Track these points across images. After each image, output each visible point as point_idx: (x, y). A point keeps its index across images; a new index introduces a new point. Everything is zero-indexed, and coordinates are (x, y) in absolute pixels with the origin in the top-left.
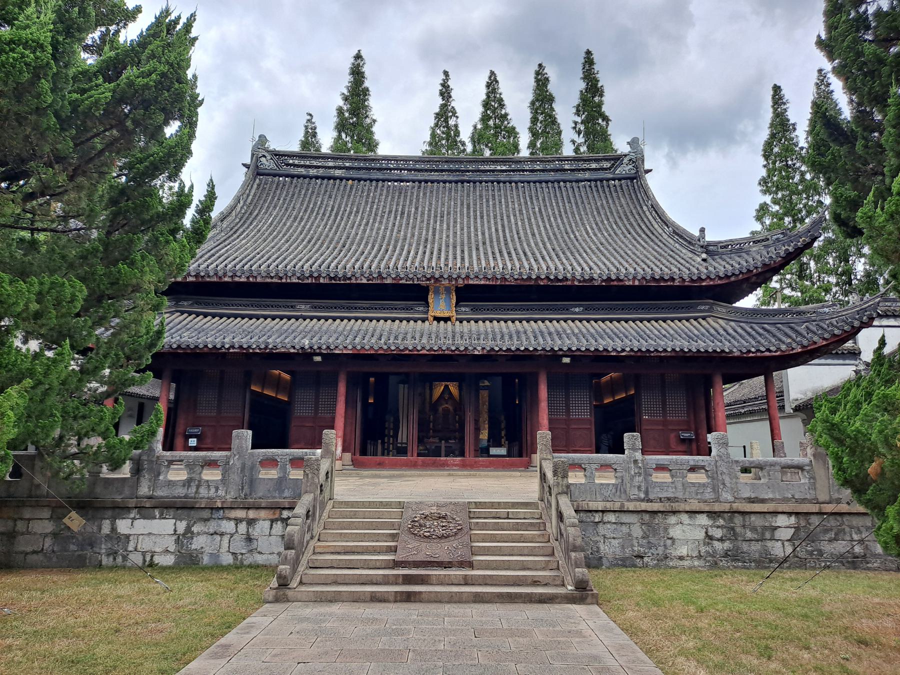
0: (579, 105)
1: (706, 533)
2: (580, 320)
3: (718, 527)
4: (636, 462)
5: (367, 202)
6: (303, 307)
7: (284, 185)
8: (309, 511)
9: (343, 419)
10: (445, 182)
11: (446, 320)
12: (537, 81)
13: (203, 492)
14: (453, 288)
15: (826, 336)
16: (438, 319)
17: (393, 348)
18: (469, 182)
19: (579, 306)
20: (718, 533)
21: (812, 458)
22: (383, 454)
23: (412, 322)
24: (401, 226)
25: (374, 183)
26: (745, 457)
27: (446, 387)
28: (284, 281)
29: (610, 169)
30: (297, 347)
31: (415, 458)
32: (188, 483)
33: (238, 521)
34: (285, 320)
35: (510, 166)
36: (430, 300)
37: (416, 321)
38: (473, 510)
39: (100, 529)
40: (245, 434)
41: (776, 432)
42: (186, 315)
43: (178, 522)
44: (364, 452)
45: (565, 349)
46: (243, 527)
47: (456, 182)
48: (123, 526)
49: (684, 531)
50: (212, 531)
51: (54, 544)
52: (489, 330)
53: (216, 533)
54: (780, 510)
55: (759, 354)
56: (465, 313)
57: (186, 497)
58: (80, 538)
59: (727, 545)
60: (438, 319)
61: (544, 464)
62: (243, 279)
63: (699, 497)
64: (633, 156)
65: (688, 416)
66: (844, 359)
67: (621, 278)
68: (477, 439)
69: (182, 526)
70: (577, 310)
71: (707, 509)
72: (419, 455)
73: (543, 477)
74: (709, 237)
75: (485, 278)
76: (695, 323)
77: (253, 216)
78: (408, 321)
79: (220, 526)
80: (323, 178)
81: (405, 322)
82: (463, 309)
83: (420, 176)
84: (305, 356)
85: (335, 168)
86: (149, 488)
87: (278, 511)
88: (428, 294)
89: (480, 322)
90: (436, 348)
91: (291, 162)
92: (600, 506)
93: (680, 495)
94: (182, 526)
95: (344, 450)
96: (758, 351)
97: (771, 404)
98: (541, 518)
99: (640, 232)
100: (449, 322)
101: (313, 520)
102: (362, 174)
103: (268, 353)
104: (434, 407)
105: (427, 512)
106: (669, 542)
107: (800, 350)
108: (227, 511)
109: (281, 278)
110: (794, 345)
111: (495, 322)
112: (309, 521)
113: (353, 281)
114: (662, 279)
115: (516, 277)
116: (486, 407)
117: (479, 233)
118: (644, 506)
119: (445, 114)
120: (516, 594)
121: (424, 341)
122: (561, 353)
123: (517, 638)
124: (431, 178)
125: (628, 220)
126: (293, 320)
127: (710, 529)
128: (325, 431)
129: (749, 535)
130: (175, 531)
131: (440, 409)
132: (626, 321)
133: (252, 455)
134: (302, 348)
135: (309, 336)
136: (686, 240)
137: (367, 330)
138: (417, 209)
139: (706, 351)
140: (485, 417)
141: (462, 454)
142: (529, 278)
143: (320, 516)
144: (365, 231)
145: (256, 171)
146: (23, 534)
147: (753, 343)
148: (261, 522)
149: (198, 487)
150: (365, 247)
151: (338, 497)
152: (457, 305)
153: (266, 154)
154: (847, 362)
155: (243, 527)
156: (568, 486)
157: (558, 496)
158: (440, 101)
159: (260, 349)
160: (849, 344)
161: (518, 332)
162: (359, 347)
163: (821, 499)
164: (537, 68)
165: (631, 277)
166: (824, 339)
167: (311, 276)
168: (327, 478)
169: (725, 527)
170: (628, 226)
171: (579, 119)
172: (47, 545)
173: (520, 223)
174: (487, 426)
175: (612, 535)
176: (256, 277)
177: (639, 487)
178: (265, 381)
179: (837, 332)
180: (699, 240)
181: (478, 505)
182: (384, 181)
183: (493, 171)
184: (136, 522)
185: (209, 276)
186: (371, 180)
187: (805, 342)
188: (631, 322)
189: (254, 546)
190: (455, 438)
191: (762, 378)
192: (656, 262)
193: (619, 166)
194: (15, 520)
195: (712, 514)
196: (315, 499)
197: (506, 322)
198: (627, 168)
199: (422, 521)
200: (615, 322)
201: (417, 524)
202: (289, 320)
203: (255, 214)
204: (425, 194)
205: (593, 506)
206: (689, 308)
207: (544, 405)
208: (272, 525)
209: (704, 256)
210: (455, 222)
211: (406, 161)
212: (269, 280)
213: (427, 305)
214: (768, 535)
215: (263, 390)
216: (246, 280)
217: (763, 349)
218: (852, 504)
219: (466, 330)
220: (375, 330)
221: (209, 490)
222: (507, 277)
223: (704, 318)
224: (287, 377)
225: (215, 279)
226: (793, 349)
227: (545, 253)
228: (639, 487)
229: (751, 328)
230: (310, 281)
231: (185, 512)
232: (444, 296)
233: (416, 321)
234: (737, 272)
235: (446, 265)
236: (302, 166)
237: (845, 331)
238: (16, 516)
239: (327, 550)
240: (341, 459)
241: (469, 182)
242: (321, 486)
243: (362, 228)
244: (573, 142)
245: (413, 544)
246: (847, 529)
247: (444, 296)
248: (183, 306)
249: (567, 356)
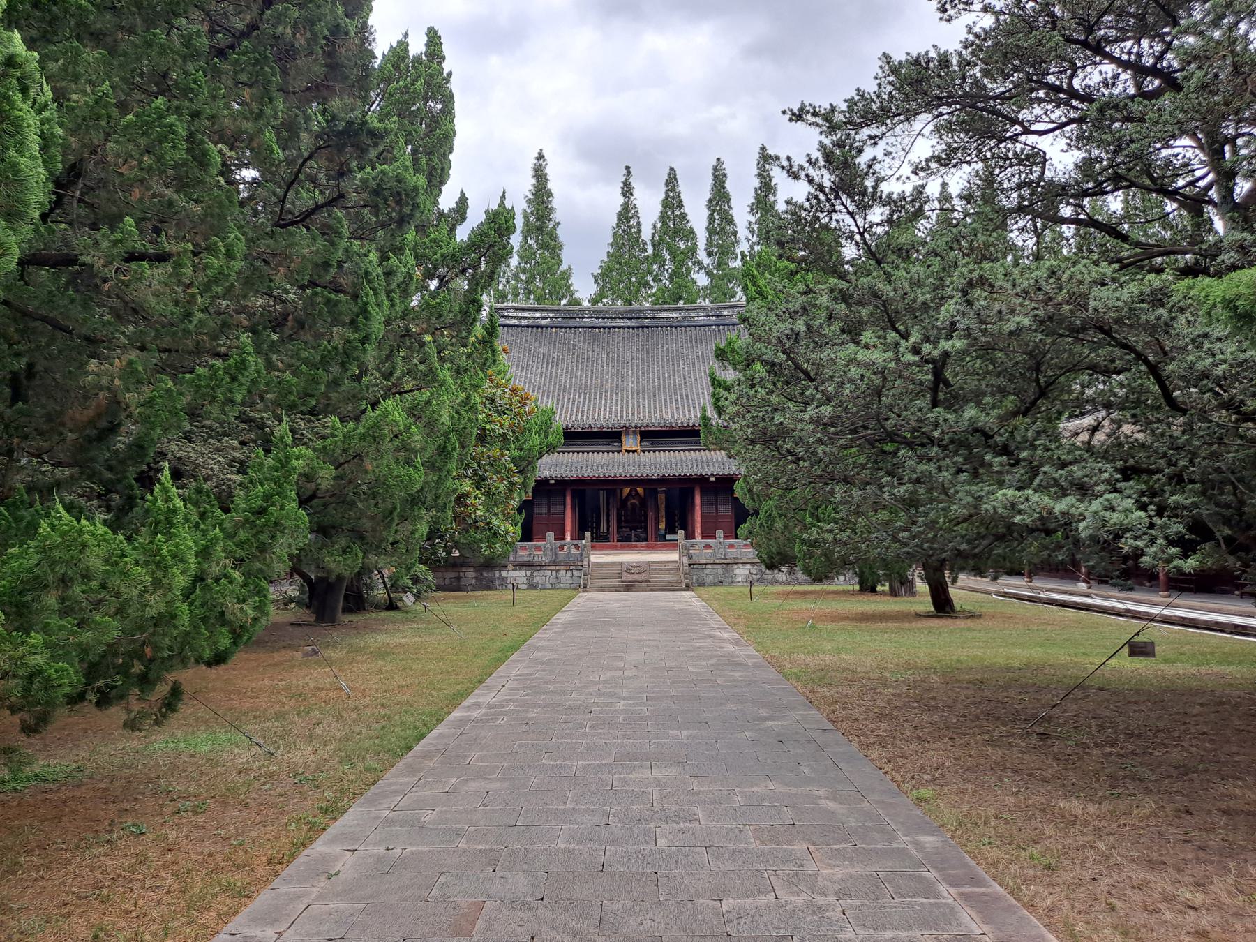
0: (753, 204)
11: (634, 452)
12: (715, 177)
16: (628, 451)
20: (755, 572)
31: (615, 543)
33: (552, 571)
38: (651, 565)
46: (554, 573)
48: (504, 574)
56: (646, 446)
59: (758, 576)
60: (628, 451)
68: (657, 529)
69: (529, 573)
80: (532, 327)
92: (705, 562)
94: (529, 573)
116: (663, 506)
118: (723, 561)
140: (663, 512)
142: (688, 426)
155: (554, 573)
158: (621, 200)
164: (715, 163)
171: (753, 219)
190: (641, 528)
205: (702, 561)
207: (698, 508)
244: (748, 240)
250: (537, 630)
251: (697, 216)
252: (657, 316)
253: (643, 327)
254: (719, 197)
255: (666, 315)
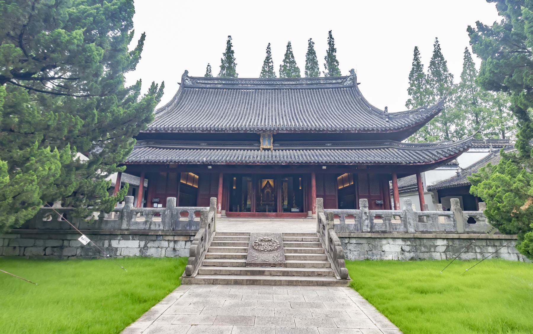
1: (402, 248)
2: (330, 150)
3: (407, 245)
4: (365, 213)
5: (232, 98)
6: (203, 144)
7: (196, 92)
8: (202, 237)
9: (221, 195)
10: (267, 89)
11: (268, 149)
13: (153, 227)
14: (272, 135)
15: (447, 155)
16: (264, 149)
17: (244, 162)
18: (278, 89)
19: (330, 143)
21: (454, 211)
22: (240, 211)
23: (253, 151)
24: (247, 109)
25: (235, 90)
26: (422, 210)
27: (268, 182)
28: (195, 132)
29: (341, 83)
30: (201, 162)
31: (254, 213)
32: (146, 222)
34: (195, 150)
35: (296, 82)
36: (261, 141)
37: (254, 150)
38: (284, 237)
39: (103, 245)
40: (173, 199)
41: (422, 200)
42: (151, 148)
43: (141, 242)
44: (231, 210)
45: (324, 162)
47: (272, 89)
48: (114, 243)
49: (390, 247)
50: (157, 246)
51: (81, 252)
52: (288, 154)
53: (159, 247)
54: (438, 237)
55: (415, 164)
57: (145, 229)
58: (94, 249)
60: (264, 149)
61: (320, 214)
62: (176, 132)
63: (397, 230)
64: (352, 77)
65: (380, 193)
66: (451, 167)
67: (350, 129)
69: (142, 244)
70: (329, 145)
71: (401, 237)
72: (256, 211)
73: (320, 221)
74: (390, 111)
75: (287, 130)
76: (383, 150)
77: (182, 105)
78: (251, 151)
79: (160, 244)
80: (213, 88)
81: (249, 151)
82: (276, 145)
83: (256, 87)
84: (204, 165)
85: (218, 84)
86: (127, 225)
87: (188, 237)
88: (260, 138)
89: (284, 151)
90: (264, 162)
91: (199, 82)
93: (388, 230)
94: (142, 244)
95: (222, 209)
96: (415, 162)
97: (420, 187)
98: (319, 241)
99: (356, 110)
100: (270, 151)
101: (205, 241)
102: (230, 87)
103: (187, 165)
104: (263, 190)
105: (262, 238)
106: (383, 253)
107: (434, 162)
108: (164, 236)
109: (193, 131)
110: (431, 160)
111: (291, 151)
112: (203, 242)
113: (226, 132)
114: (368, 130)
115: (301, 129)
116: (286, 190)
117: (283, 111)
119: (268, 60)
120: (309, 281)
121: (259, 158)
122: (322, 164)
123: (315, 309)
124: (261, 88)
125: (350, 105)
126: (199, 150)
127: (403, 247)
128: (211, 198)
129: (423, 249)
130: (139, 246)
131: (265, 191)
132: (352, 150)
133: (177, 209)
134: (203, 162)
135: (206, 157)
136: (378, 113)
137: (232, 154)
138: (254, 101)
139: (390, 163)
140: (286, 194)
141: (275, 211)
143: (209, 240)
144: (231, 111)
145: (183, 85)
146: (67, 247)
147: (412, 159)
148: (181, 242)
149: (150, 225)
150: (232, 117)
151: (218, 230)
152: (273, 143)
153: (188, 78)
154: (453, 168)
156: (334, 225)
157: (329, 230)
159: (184, 163)
160: (454, 161)
161: (302, 155)
162: (228, 162)
163: (459, 232)
165: (354, 129)
166: (446, 157)
167: (207, 130)
168: (212, 221)
169: (411, 246)
170: (351, 108)
172: (78, 253)
173: (301, 107)
174: (287, 199)
175: (354, 250)
176: (182, 131)
177: (367, 226)
178: (188, 178)
179: (452, 153)
180: (385, 112)
181: (286, 234)
182: (240, 89)
183: (289, 84)
184: (121, 242)
185: (161, 130)
186: (234, 89)
187: (437, 159)
188: (354, 150)
189: (177, 254)
191: (416, 175)
192: (365, 122)
193: (345, 82)
194: (63, 240)
195: (404, 239)
196: (206, 231)
197: (296, 150)
198: (349, 83)
199: (259, 243)
200: (346, 150)
201: (257, 244)
202: (197, 150)
203: (183, 104)
204: (258, 95)
206: (380, 144)
208: (186, 244)
209: (387, 119)
210: (272, 107)
211: (250, 80)
212: (188, 132)
213: (260, 143)
214: (433, 250)
215: (187, 182)
216: (177, 132)
217: (417, 162)
218: (490, 233)
219: (278, 154)
220: (235, 154)
221: (156, 226)
222: (297, 129)
223: (387, 148)
224: (197, 177)
225: (164, 131)
226: (431, 161)
227: (313, 119)
228: (367, 226)
229: (410, 152)
230: (206, 132)
231: (144, 237)
232: (267, 139)
233: (254, 150)
234: (403, 126)
235: (268, 125)
236: (204, 83)
237: (456, 153)
238: (64, 238)
239: (211, 257)
240: (220, 213)
241: (278, 89)
242: (209, 225)
243: (230, 109)
244: (324, 72)
245: (256, 254)
246: (473, 247)
247: (267, 139)
248: (150, 144)
249: (324, 166)
250: (134, 321)
251: (301, 62)
252: (284, 83)
253: (275, 89)
254: (311, 52)
255: (288, 83)
